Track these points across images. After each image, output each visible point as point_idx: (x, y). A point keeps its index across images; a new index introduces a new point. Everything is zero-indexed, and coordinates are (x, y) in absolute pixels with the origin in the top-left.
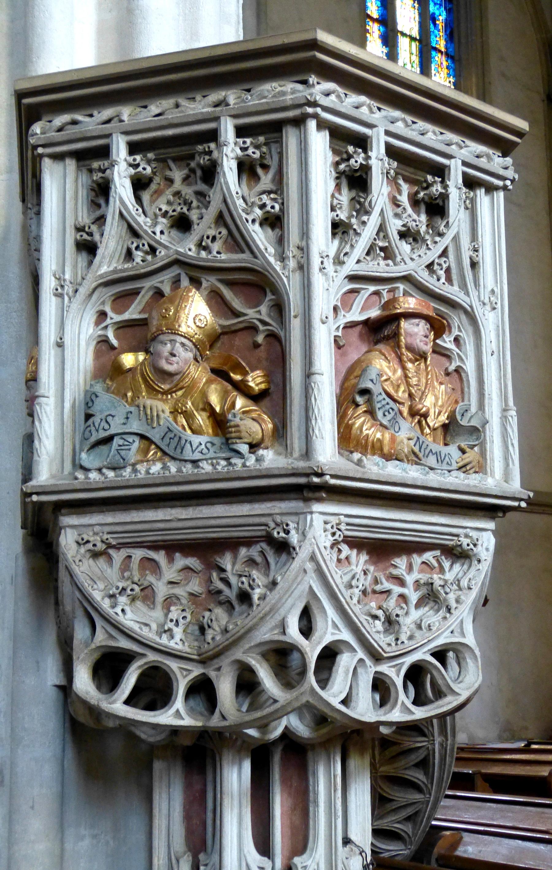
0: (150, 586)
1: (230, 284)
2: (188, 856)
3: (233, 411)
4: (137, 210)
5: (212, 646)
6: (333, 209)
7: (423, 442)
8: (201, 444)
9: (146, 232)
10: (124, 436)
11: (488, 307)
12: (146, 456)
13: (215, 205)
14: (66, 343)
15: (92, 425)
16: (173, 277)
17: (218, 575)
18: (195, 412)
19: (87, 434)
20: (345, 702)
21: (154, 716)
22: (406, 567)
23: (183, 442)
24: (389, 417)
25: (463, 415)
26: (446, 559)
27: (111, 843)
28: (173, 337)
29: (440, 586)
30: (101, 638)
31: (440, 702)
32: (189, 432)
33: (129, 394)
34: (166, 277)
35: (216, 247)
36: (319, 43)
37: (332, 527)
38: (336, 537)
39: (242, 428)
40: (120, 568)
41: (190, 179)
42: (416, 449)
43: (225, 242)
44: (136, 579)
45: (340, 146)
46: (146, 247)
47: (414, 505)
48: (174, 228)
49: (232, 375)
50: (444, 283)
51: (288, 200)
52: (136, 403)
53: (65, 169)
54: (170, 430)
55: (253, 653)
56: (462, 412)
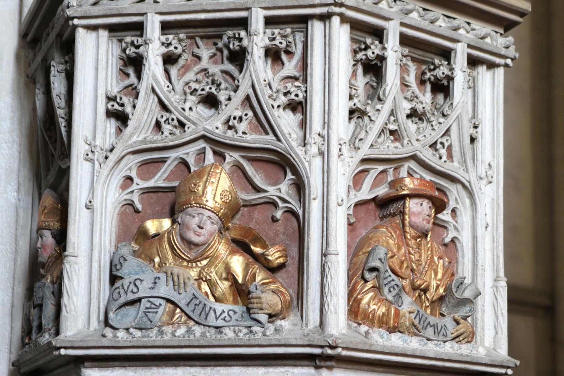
1: (250, 159)
3: (254, 283)
4: (168, 87)
6: (351, 98)
7: (423, 315)
8: (224, 312)
10: (151, 299)
11: (485, 181)
12: (172, 320)
13: (245, 89)
14: (95, 206)
15: (121, 287)
16: (198, 150)
18: (219, 281)
19: (116, 295)
23: (207, 309)
24: (394, 293)
25: (458, 287)
32: (212, 298)
33: (157, 260)
34: (191, 150)
35: (242, 127)
39: (263, 300)
41: (216, 57)
42: (416, 322)
43: (250, 123)
45: (360, 36)
46: (175, 122)
48: (201, 104)
49: (252, 247)
50: (445, 161)
54: (195, 297)
56: (457, 284)
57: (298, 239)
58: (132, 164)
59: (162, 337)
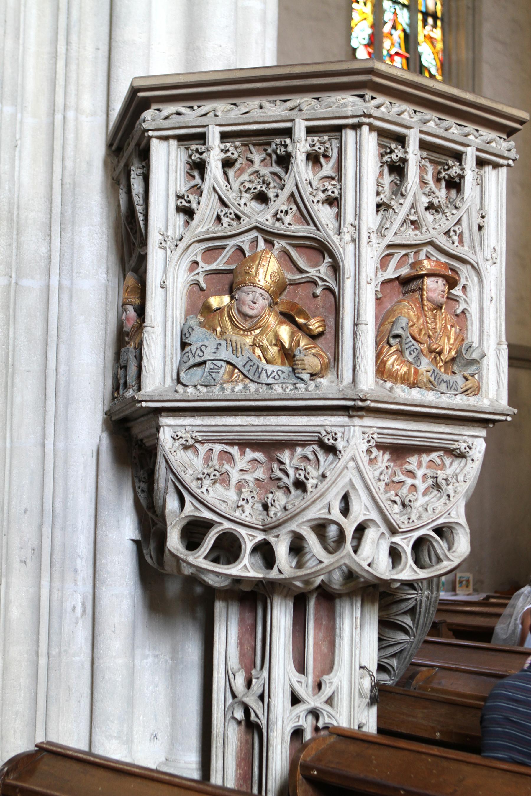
0: (227, 472)
1: (294, 246)
2: (242, 672)
3: (298, 348)
5: (274, 519)
6: (378, 194)
9: (233, 204)
10: (214, 362)
12: (231, 378)
13: (290, 187)
17: (279, 467)
18: (269, 347)
20: (369, 565)
21: (228, 569)
22: (418, 464)
23: (260, 369)
24: (414, 355)
26: (448, 458)
27: (170, 661)
28: (254, 289)
29: (443, 479)
30: (189, 509)
31: (438, 567)
32: (264, 361)
33: (219, 329)
34: (246, 238)
35: (288, 219)
36: (375, 70)
37: (368, 437)
38: (371, 444)
39: (306, 362)
40: (204, 458)
42: (432, 379)
43: (294, 215)
44: (217, 468)
45: (385, 142)
46: (233, 216)
47: (427, 419)
49: (297, 319)
50: (457, 246)
51: (345, 188)
52: (225, 338)
53: (169, 146)
54: (250, 360)
55: (304, 526)
56: (467, 348)
57: (334, 312)
58: (197, 250)
59: (223, 392)
